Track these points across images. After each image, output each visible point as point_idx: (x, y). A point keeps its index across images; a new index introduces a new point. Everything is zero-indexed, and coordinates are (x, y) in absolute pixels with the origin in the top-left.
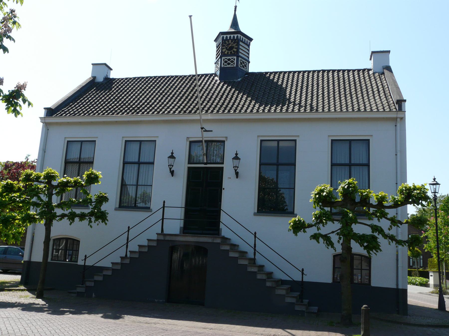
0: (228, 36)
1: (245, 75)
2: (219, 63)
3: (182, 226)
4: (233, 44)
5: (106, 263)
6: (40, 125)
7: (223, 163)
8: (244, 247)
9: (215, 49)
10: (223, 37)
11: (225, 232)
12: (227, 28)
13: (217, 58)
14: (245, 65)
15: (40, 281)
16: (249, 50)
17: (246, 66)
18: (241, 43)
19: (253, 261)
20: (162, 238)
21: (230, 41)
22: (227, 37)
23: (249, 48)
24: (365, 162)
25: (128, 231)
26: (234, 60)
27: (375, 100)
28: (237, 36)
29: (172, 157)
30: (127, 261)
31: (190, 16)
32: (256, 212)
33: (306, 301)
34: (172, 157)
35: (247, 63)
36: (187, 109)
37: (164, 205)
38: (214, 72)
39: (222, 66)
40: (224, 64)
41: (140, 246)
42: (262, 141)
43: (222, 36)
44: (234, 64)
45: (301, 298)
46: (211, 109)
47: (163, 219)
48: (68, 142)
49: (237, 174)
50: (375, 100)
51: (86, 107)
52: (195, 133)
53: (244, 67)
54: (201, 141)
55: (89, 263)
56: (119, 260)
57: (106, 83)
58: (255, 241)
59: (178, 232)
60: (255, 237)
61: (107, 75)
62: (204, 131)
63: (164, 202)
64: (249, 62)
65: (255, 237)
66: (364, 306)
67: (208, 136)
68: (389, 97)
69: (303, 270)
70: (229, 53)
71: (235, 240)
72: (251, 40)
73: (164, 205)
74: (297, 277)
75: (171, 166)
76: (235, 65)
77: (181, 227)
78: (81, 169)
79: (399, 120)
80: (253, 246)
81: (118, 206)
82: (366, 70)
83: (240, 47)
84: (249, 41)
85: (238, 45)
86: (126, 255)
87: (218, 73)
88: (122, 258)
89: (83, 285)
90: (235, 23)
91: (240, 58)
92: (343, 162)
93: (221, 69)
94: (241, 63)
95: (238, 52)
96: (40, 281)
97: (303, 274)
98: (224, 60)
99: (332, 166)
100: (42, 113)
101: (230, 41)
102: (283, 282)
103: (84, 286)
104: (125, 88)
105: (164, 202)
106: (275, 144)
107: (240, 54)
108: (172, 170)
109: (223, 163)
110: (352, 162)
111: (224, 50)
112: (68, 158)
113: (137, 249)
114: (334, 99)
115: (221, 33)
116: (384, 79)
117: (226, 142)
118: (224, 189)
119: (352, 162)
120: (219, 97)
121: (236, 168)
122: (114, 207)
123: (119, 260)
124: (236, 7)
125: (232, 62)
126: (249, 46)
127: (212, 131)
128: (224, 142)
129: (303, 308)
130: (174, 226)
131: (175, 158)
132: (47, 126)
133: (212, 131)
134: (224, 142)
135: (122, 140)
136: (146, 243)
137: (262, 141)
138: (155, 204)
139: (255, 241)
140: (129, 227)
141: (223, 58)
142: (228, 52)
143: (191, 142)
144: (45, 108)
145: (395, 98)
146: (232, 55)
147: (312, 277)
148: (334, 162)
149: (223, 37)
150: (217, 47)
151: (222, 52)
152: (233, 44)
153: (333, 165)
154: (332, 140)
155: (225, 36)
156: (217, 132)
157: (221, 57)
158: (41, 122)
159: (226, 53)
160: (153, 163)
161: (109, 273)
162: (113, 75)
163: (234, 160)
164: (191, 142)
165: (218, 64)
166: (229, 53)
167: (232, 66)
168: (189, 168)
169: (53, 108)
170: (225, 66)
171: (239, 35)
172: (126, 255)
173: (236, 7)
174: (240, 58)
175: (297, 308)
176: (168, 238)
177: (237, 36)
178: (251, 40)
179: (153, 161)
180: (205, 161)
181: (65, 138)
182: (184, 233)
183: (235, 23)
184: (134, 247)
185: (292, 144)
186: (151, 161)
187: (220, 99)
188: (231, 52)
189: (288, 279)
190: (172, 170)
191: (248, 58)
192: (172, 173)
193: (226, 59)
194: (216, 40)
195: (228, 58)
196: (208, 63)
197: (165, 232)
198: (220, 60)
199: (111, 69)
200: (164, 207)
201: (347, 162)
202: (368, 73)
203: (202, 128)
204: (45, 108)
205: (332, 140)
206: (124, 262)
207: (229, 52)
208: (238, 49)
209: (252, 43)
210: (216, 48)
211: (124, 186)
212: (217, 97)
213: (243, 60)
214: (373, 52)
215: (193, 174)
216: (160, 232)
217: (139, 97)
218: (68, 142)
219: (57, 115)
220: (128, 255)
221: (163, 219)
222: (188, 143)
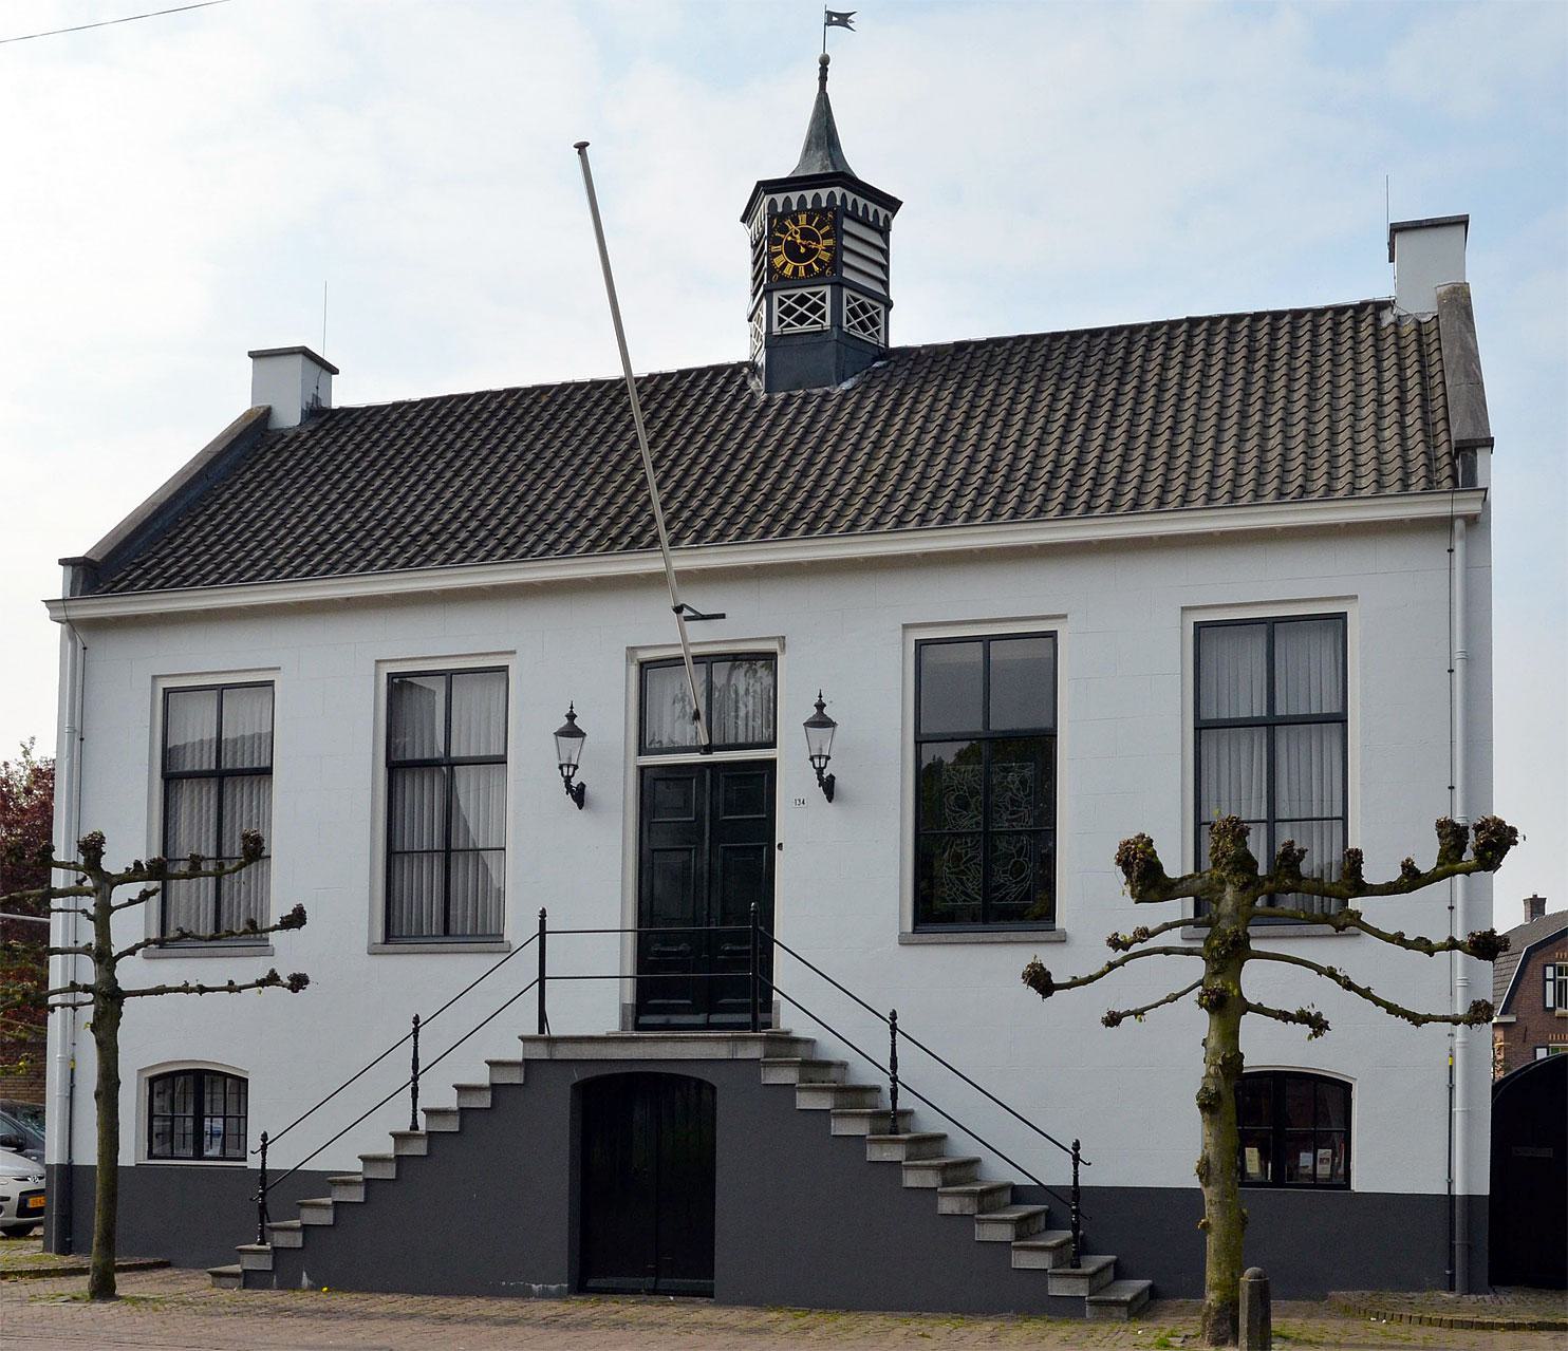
0: (794, 196)
1: (875, 360)
2: (764, 316)
3: (630, 998)
4: (820, 225)
5: (344, 1159)
6: (53, 633)
7: (772, 745)
8: (866, 1074)
9: (747, 255)
10: (773, 203)
11: (788, 1019)
12: (785, 164)
13: (755, 295)
14: (856, 316)
15: (95, 1239)
16: (885, 253)
17: (875, 324)
18: (848, 225)
19: (893, 1121)
20: (540, 1052)
21: (803, 218)
22: (787, 201)
23: (887, 242)
24: (1330, 707)
25: (416, 1031)
26: (823, 299)
27: (1379, 441)
28: (832, 196)
29: (571, 731)
30: (419, 1148)
31: (582, 147)
32: (909, 928)
33: (1092, 1263)
34: (571, 731)
35: (882, 308)
36: (623, 532)
37: (542, 924)
38: (746, 358)
39: (776, 329)
40: (781, 321)
41: (461, 1089)
42: (920, 644)
43: (767, 200)
44: (823, 317)
45: (1071, 1256)
46: (720, 523)
47: (542, 979)
48: (167, 692)
49: (828, 786)
50: (1379, 441)
51: (400, 536)
52: (654, 626)
53: (865, 329)
54: (677, 661)
55: (281, 1159)
56: (387, 1148)
57: (313, 433)
58: (894, 1042)
59: (617, 1030)
60: (894, 1028)
61: (316, 398)
62: (687, 619)
63: (543, 914)
64: (889, 305)
65: (894, 1028)
66: (1249, 1271)
67: (705, 638)
68: (1441, 426)
69: (1077, 1146)
70: (802, 272)
71: (831, 1048)
72: (893, 205)
73: (542, 924)
74: (1057, 1173)
75: (568, 768)
76: (827, 323)
77: (624, 1006)
78: (228, 802)
79: (1459, 525)
80: (887, 1065)
81: (379, 936)
82: (1370, 309)
83: (847, 242)
84: (882, 213)
85: (837, 233)
86: (415, 1126)
87: (761, 360)
88: (398, 1137)
89: (263, 1243)
90: (824, 133)
91: (846, 292)
92: (1244, 714)
93: (773, 343)
94: (852, 311)
95: (836, 264)
96: (95, 1239)
97: (1076, 1158)
98: (781, 303)
99: (1198, 729)
100: (56, 583)
101: (803, 218)
102: (1018, 1194)
103: (268, 1247)
104: (386, 448)
105: (543, 914)
106: (975, 653)
107: (847, 274)
108: (575, 783)
109: (772, 745)
110: (1280, 711)
111: (778, 261)
112: (1204, 716)
113: (450, 1101)
114: (1195, 443)
115: (765, 187)
116: (1435, 345)
117: (782, 662)
118: (780, 845)
119: (1280, 711)
120: (758, 467)
121: (819, 760)
122: (364, 943)
123: (387, 1148)
124: (825, 62)
125: (789, 311)
126: (884, 232)
127: (723, 616)
128: (769, 658)
129: (1081, 1289)
130: (594, 1003)
131: (581, 734)
132: (82, 631)
133: (723, 616)
134: (769, 658)
135: (377, 676)
136: (482, 1077)
137: (920, 644)
138: (518, 926)
139: (894, 1042)
140: (416, 1020)
141: (776, 296)
142: (796, 269)
143: (644, 666)
144: (63, 562)
145: (1460, 430)
146: (813, 278)
147: (1113, 1167)
148: (1210, 714)
149: (773, 203)
150: (754, 247)
151: (771, 269)
152: (820, 225)
153: (1201, 727)
154: (1199, 626)
155: (780, 198)
156: (745, 620)
157: (768, 293)
158: (52, 619)
159: (788, 271)
160: (501, 760)
161: (357, 1195)
162: (344, 394)
163: (809, 729)
164: (644, 666)
165: (759, 321)
166: (802, 272)
167: (817, 327)
168: (642, 769)
169: (98, 559)
170: (787, 331)
171: (838, 191)
172: (415, 1126)
173: (825, 62)
174: (846, 292)
175: (1057, 1288)
176: (563, 1052)
177: (832, 196)
178: (893, 205)
179: (502, 753)
180: (704, 741)
181: (154, 678)
182: (638, 1027)
183: (824, 133)
184: (439, 1093)
185: (1041, 648)
186: (496, 750)
187: (761, 477)
188: (809, 269)
189: (1020, 1180)
190: (575, 783)
191: (885, 284)
192: (579, 795)
193: (789, 297)
194: (746, 217)
195: (799, 292)
196: (704, 317)
197: (555, 1029)
198: (764, 302)
199: (335, 371)
200: (542, 933)
201: (1260, 710)
202: (1378, 320)
203: (678, 610)
204: (63, 562)
205: (1199, 626)
206: (400, 1154)
207: (801, 266)
208: (837, 250)
209: (897, 223)
210: (750, 250)
211: (397, 858)
212: (748, 467)
213: (863, 299)
214: (1396, 229)
215: (660, 790)
216: (535, 1032)
217: (549, 474)
218: (167, 692)
219: (116, 584)
220: (422, 1127)
221: (542, 979)
222: (634, 670)
